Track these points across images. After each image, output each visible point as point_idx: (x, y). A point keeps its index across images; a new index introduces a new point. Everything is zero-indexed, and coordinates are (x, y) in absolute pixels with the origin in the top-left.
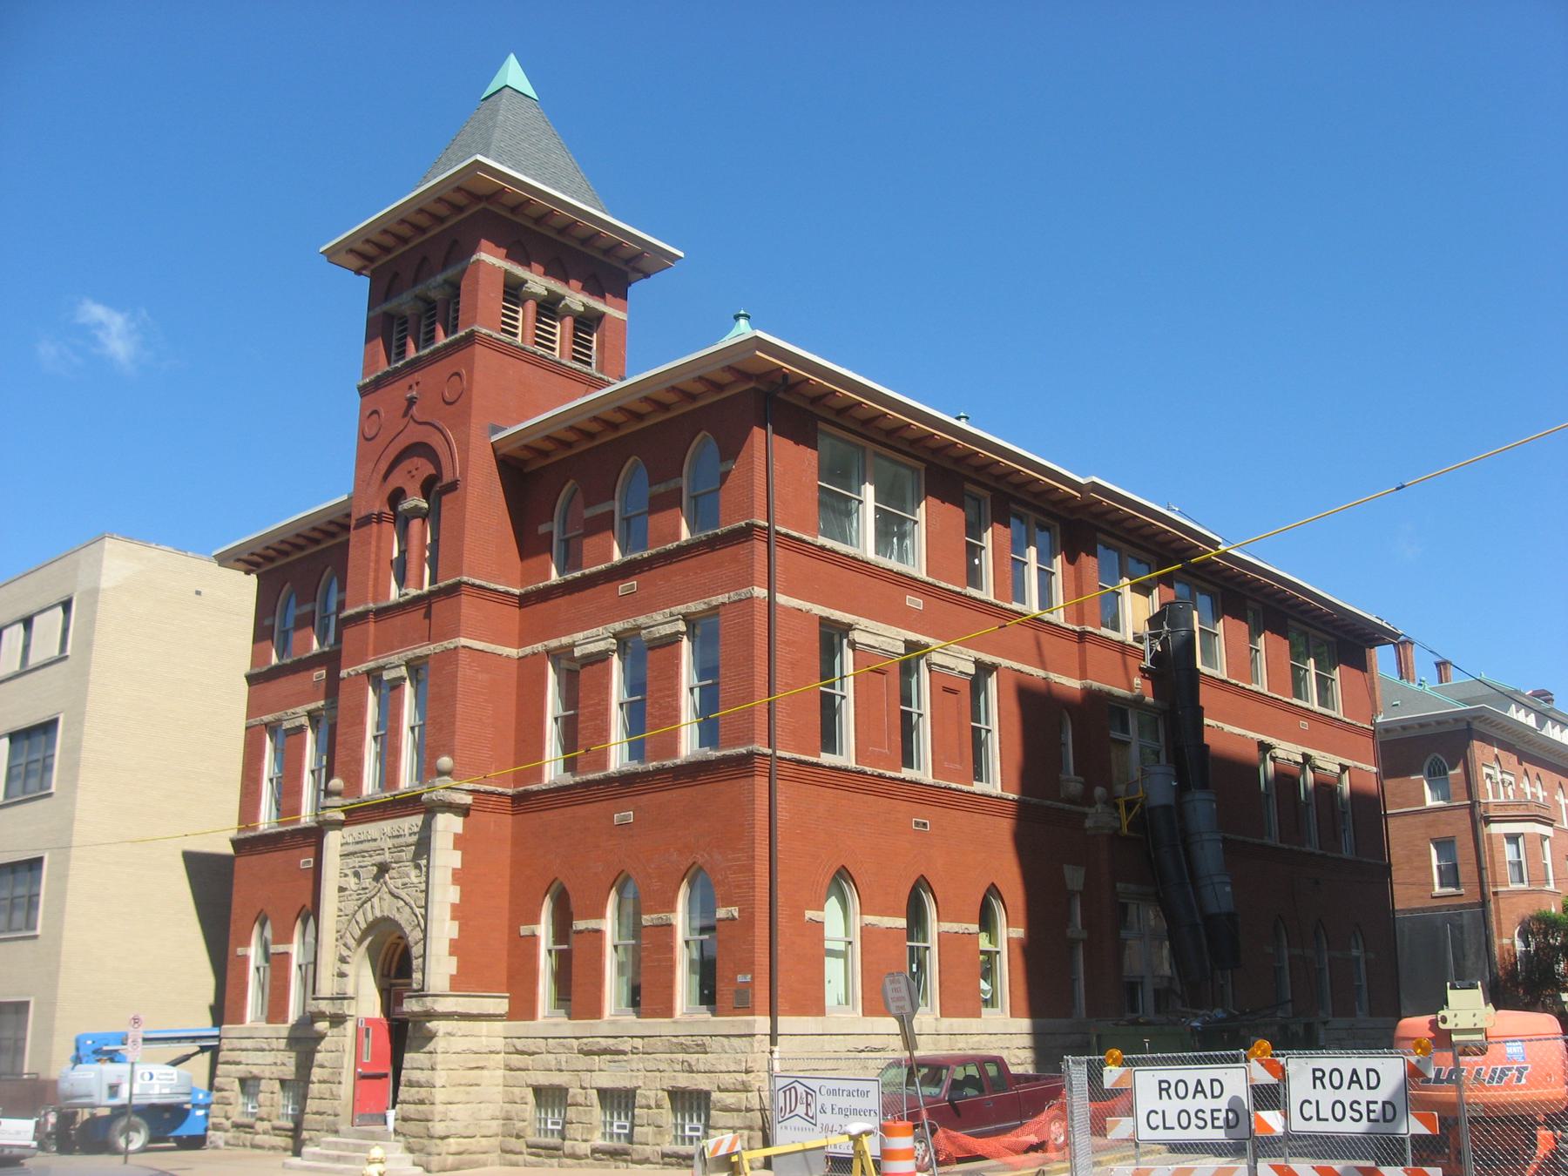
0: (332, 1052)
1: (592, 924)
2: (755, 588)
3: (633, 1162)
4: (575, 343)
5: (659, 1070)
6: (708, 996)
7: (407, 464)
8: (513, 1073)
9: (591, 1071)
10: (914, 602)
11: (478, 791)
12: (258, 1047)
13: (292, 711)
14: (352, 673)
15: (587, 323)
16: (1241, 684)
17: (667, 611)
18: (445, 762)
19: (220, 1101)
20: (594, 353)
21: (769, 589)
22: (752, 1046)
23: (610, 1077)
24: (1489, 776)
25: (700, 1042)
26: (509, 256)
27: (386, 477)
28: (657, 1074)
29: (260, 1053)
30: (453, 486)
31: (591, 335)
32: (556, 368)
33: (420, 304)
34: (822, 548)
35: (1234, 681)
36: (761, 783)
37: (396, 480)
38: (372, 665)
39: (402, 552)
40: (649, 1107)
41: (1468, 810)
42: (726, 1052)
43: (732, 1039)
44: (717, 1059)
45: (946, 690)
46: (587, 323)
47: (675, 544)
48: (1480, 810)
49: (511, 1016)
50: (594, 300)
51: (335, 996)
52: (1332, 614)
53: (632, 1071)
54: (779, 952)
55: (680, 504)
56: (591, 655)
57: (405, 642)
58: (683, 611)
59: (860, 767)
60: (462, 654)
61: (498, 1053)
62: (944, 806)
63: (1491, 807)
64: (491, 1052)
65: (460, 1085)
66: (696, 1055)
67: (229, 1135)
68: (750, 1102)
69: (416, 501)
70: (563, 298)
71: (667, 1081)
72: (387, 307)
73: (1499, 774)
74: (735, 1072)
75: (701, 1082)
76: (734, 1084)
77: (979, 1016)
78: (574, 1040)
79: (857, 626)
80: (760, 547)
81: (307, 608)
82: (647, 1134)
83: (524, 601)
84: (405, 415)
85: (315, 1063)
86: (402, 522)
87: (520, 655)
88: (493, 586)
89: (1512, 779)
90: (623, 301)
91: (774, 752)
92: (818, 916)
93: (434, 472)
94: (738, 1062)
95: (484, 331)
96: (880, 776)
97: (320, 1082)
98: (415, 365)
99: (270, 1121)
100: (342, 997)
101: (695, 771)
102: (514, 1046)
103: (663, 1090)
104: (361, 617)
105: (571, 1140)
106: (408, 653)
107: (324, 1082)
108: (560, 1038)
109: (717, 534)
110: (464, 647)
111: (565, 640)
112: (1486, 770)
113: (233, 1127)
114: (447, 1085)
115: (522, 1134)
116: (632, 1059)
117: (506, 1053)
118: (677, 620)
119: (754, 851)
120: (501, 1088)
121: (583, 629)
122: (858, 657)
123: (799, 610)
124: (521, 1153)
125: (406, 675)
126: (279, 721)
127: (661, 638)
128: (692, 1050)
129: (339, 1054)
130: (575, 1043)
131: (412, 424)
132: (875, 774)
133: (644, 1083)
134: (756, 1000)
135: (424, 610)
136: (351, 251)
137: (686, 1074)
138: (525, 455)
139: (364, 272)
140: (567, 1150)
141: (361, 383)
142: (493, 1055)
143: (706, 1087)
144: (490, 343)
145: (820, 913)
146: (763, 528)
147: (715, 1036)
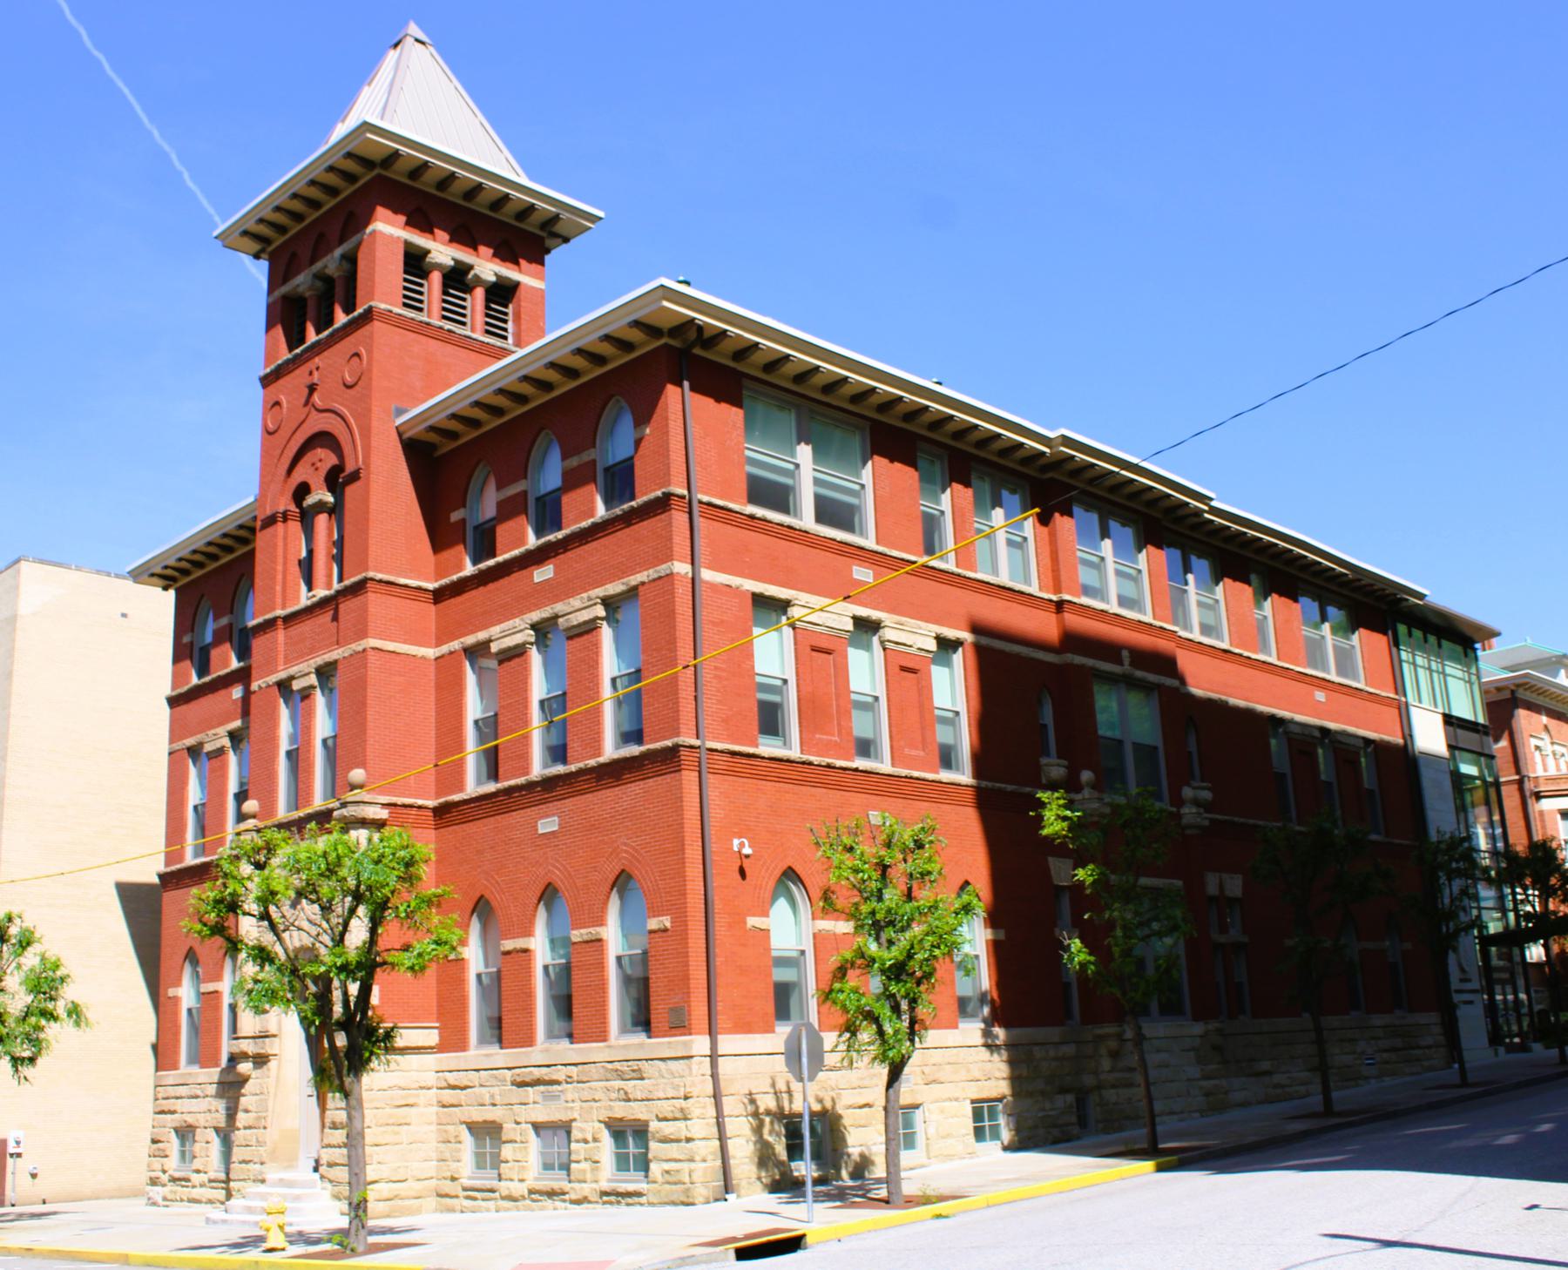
0: (257, 1094)
1: (519, 943)
2: (676, 563)
4: (488, 315)
5: (594, 1100)
6: (643, 1020)
7: (309, 457)
8: (445, 1109)
9: (525, 1104)
10: (863, 574)
11: (395, 805)
12: (192, 1094)
13: (213, 731)
14: (263, 685)
15: (502, 293)
16: (1246, 654)
17: (585, 595)
18: (357, 775)
19: (156, 1154)
20: (510, 326)
21: (693, 563)
22: (690, 1069)
24: (1537, 748)
25: (636, 1068)
26: (411, 223)
27: (290, 471)
28: (593, 1104)
29: (195, 1100)
30: (355, 476)
31: (506, 307)
32: (466, 343)
33: (319, 284)
34: (752, 517)
35: (1237, 651)
36: (689, 778)
37: (301, 474)
38: (282, 675)
39: (310, 552)
40: (586, 1141)
41: (1516, 786)
42: (663, 1077)
43: (669, 1062)
44: (654, 1085)
45: (904, 669)
46: (502, 293)
47: (590, 521)
48: (1529, 786)
49: (442, 1048)
50: (508, 268)
51: (258, 1034)
52: (1346, 575)
53: (567, 1102)
54: (718, 963)
55: (595, 481)
56: (509, 649)
57: (313, 651)
58: (601, 595)
59: (805, 757)
60: (372, 657)
61: (429, 1089)
62: (905, 797)
63: (1541, 781)
64: (421, 1088)
65: (388, 1125)
66: (633, 1082)
67: (166, 1190)
68: (690, 1131)
69: (323, 495)
70: (471, 267)
71: (603, 1111)
72: (284, 289)
73: (1549, 745)
74: (673, 1098)
75: (637, 1111)
76: (672, 1112)
77: (956, 1027)
78: (506, 1071)
79: (796, 602)
80: (679, 518)
81: (224, 621)
82: (584, 1171)
83: (439, 596)
84: (306, 404)
85: (241, 1107)
86: (306, 518)
87: (438, 654)
88: (403, 581)
89: (1563, 750)
90: (540, 267)
91: (704, 743)
92: (763, 922)
93: (337, 462)
94: (676, 1087)
95: (383, 306)
96: (829, 766)
97: (245, 1128)
98: (318, 348)
99: (206, 1173)
100: (264, 1036)
101: (616, 772)
102: (446, 1080)
103: (600, 1121)
104: (270, 625)
106: (317, 659)
107: (250, 1127)
108: (492, 1069)
109: (632, 507)
110: (373, 648)
111: (482, 636)
112: (1534, 742)
113: (170, 1181)
114: (373, 1125)
115: (456, 1176)
116: (566, 1090)
117: (438, 1088)
118: (595, 604)
119: (684, 854)
120: (434, 1128)
121: (500, 622)
122: (799, 637)
123: (728, 586)
124: (457, 1197)
125: (316, 683)
126: (201, 744)
127: (579, 625)
129: (262, 1097)
130: (508, 1074)
131: (314, 412)
132: (823, 764)
133: (580, 1115)
134: (693, 1017)
135: (332, 612)
136: (245, 233)
137: (623, 1103)
138: (433, 437)
139: (263, 255)
141: (262, 373)
142: (424, 1091)
143: (643, 1117)
144: (388, 317)
145: (764, 919)
146: (683, 497)
147: (652, 1060)
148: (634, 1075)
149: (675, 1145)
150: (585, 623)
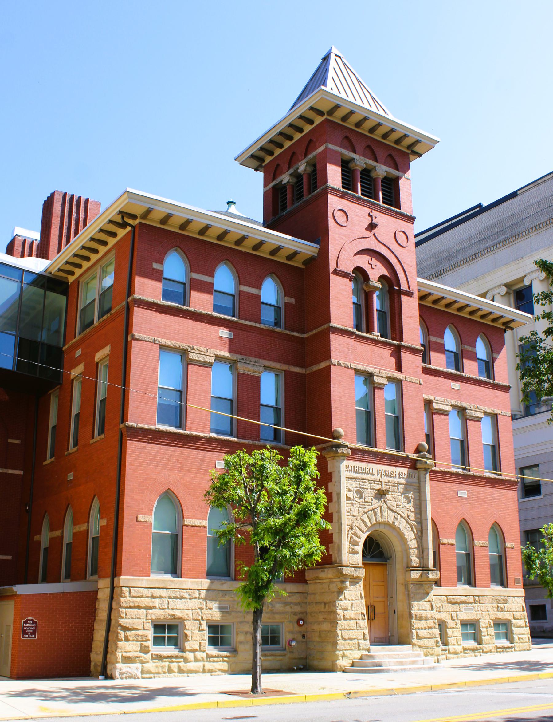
3: (483, 652)
23: (466, 614)
105: (452, 645)
108: (437, 595)
128: (501, 602)
139: (259, 169)
140: (451, 651)
148: (503, 602)
149: (522, 628)
150: (478, 417)
